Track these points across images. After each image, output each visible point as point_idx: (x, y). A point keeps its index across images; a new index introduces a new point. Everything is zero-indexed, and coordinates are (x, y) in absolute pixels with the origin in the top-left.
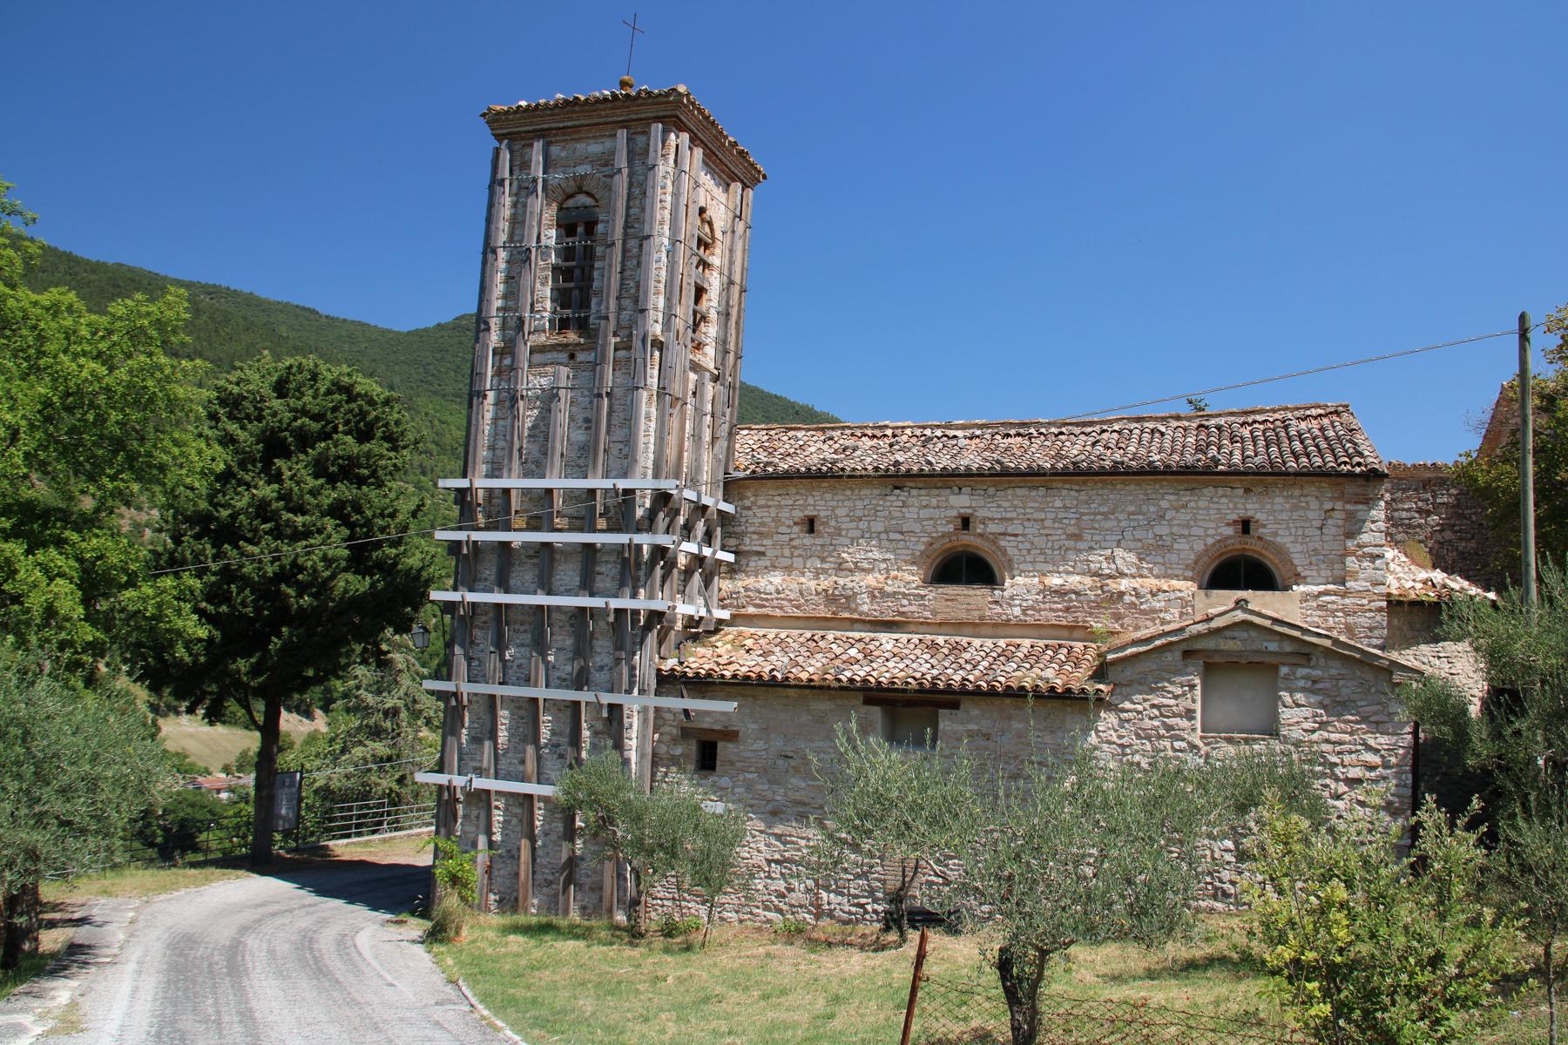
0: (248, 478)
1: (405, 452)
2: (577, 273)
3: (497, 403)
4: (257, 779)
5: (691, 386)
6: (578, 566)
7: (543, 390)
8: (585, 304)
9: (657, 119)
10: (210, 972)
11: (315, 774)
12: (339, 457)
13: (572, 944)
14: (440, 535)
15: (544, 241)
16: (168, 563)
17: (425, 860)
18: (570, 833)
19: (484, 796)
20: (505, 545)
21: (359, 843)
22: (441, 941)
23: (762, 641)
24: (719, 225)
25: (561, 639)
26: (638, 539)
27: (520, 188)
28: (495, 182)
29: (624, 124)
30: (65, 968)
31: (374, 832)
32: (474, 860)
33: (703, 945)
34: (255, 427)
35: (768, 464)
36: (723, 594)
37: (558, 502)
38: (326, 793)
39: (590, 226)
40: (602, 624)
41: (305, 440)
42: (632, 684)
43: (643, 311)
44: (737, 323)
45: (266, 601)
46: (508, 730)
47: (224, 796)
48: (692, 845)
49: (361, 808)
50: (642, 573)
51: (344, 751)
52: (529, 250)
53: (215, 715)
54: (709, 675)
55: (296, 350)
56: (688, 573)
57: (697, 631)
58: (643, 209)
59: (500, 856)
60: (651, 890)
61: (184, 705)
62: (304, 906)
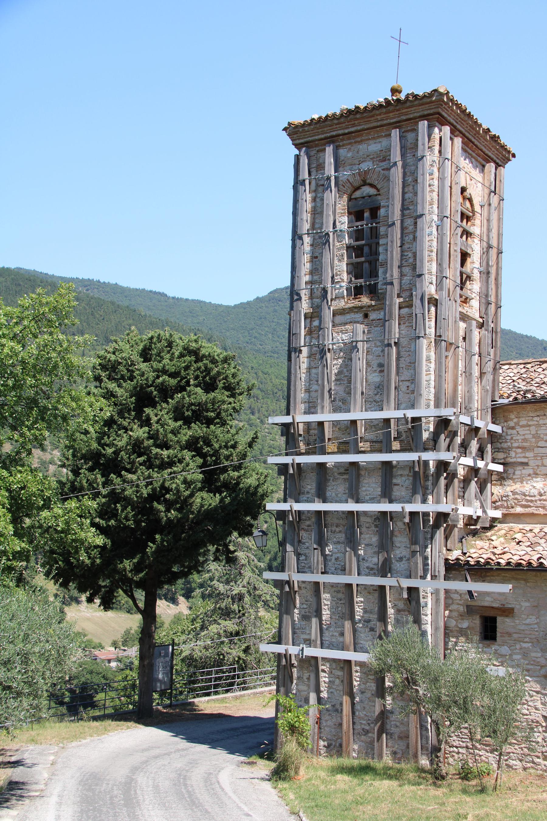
0: (125, 423)
1: (240, 398)
2: (366, 250)
3: (310, 356)
4: (141, 650)
5: (462, 333)
6: (379, 479)
7: (345, 344)
8: (374, 274)
9: (423, 117)
10: (112, 803)
11: (183, 647)
12: (192, 404)
13: (387, 783)
14: (272, 460)
15: (339, 226)
16: (70, 491)
17: (269, 713)
18: (381, 691)
19: (313, 662)
20: (322, 466)
21: (218, 700)
22: (284, 779)
23: (530, 535)
24: (477, 201)
25: (368, 538)
26: (426, 456)
27: (317, 185)
28: (298, 183)
29: (396, 125)
30: (7, 800)
31: (227, 691)
32: (307, 713)
33: (495, 788)
34: (129, 385)
35: (526, 392)
36: (495, 498)
37: (361, 430)
38: (190, 661)
39: (374, 211)
40: (400, 524)
41: (166, 393)
42: (425, 571)
43: (420, 276)
44: (496, 279)
45: (143, 515)
46: (330, 609)
47: (113, 664)
48: (481, 701)
49: (217, 672)
50: (430, 483)
51: (203, 628)
52: (327, 234)
53: (108, 604)
54: (487, 563)
55: (153, 325)
56: (466, 482)
57: (474, 528)
58: (416, 194)
59: (327, 710)
60: (450, 740)
61: (83, 598)
62: (178, 750)
